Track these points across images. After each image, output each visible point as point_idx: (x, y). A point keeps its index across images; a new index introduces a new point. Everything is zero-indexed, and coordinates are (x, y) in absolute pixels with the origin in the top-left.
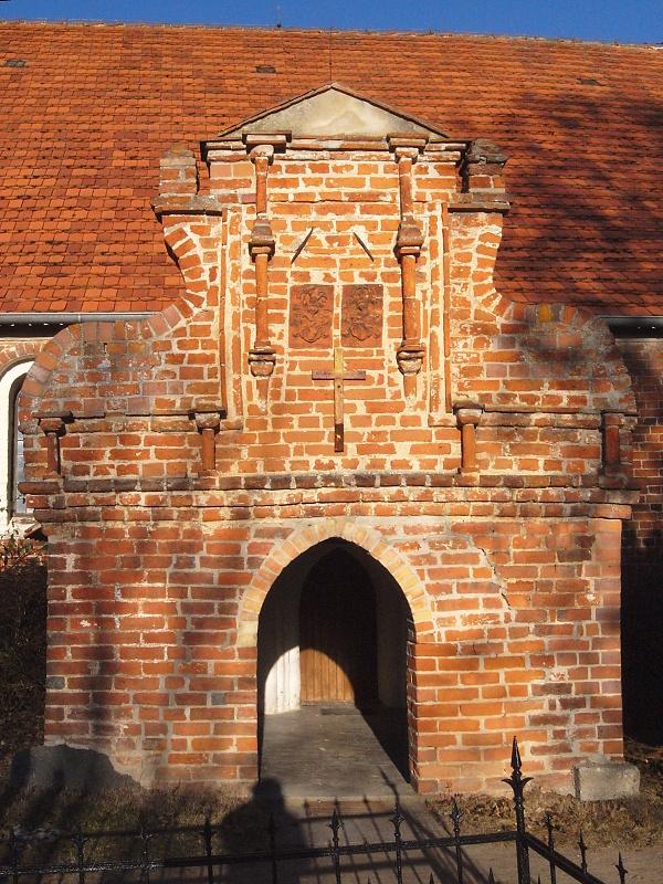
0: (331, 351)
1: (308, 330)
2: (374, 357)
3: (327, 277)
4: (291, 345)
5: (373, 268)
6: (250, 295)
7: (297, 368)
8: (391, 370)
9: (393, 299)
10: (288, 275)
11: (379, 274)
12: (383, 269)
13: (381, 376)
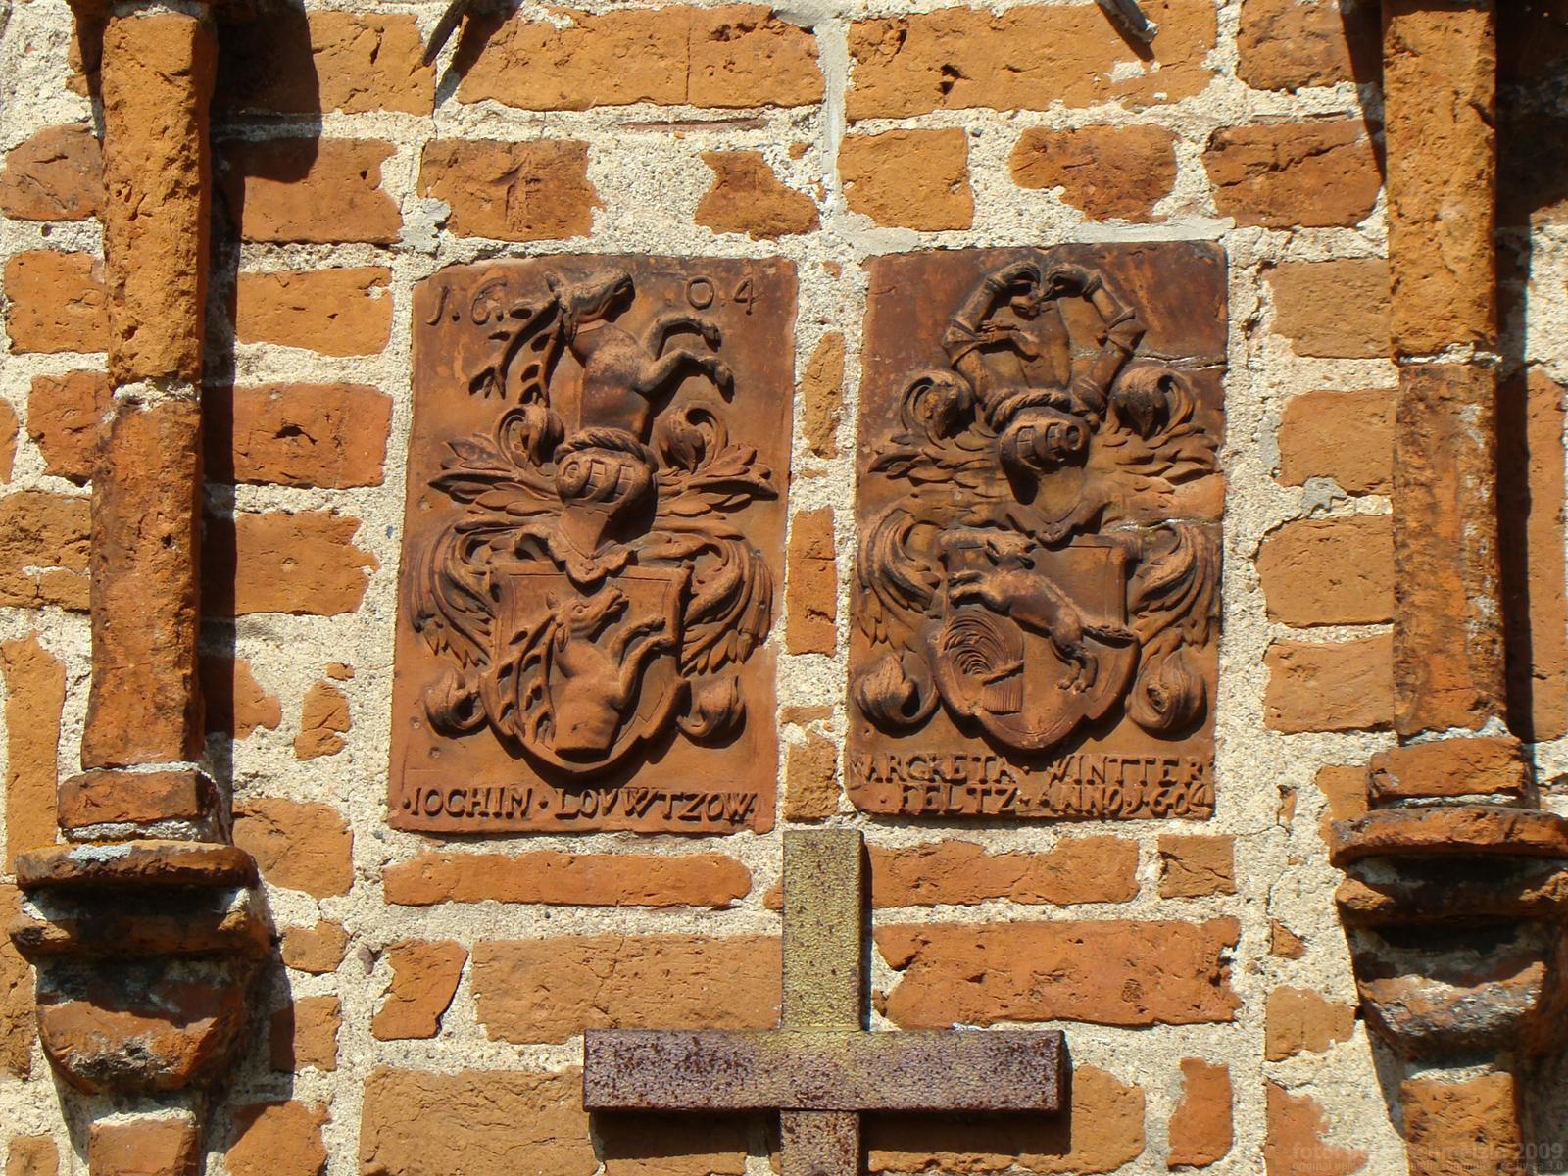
0: (760, 854)
1: (584, 723)
2: (1145, 908)
3: (738, 184)
4: (419, 809)
5: (1136, 95)
6: (59, 365)
7: (463, 1011)
8: (1295, 1029)
9: (1313, 375)
10: (398, 177)
11: (1189, 153)
12: (1228, 99)
13: (1208, 1085)
